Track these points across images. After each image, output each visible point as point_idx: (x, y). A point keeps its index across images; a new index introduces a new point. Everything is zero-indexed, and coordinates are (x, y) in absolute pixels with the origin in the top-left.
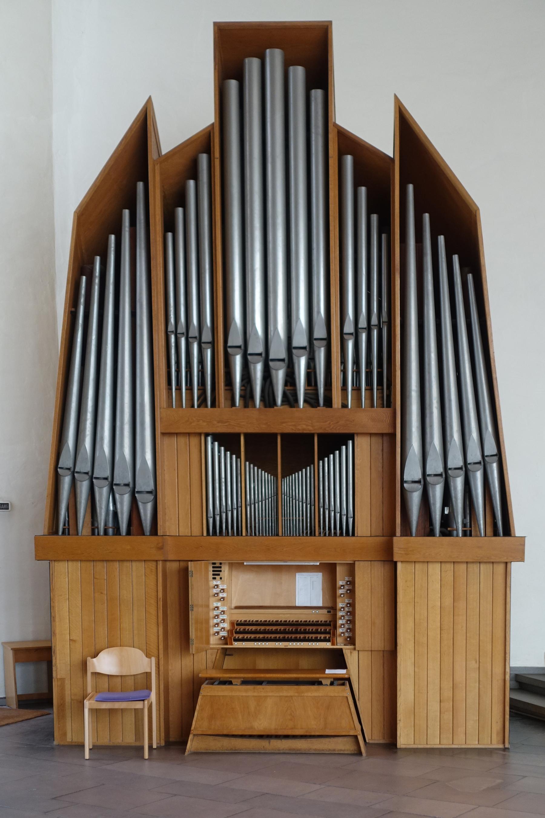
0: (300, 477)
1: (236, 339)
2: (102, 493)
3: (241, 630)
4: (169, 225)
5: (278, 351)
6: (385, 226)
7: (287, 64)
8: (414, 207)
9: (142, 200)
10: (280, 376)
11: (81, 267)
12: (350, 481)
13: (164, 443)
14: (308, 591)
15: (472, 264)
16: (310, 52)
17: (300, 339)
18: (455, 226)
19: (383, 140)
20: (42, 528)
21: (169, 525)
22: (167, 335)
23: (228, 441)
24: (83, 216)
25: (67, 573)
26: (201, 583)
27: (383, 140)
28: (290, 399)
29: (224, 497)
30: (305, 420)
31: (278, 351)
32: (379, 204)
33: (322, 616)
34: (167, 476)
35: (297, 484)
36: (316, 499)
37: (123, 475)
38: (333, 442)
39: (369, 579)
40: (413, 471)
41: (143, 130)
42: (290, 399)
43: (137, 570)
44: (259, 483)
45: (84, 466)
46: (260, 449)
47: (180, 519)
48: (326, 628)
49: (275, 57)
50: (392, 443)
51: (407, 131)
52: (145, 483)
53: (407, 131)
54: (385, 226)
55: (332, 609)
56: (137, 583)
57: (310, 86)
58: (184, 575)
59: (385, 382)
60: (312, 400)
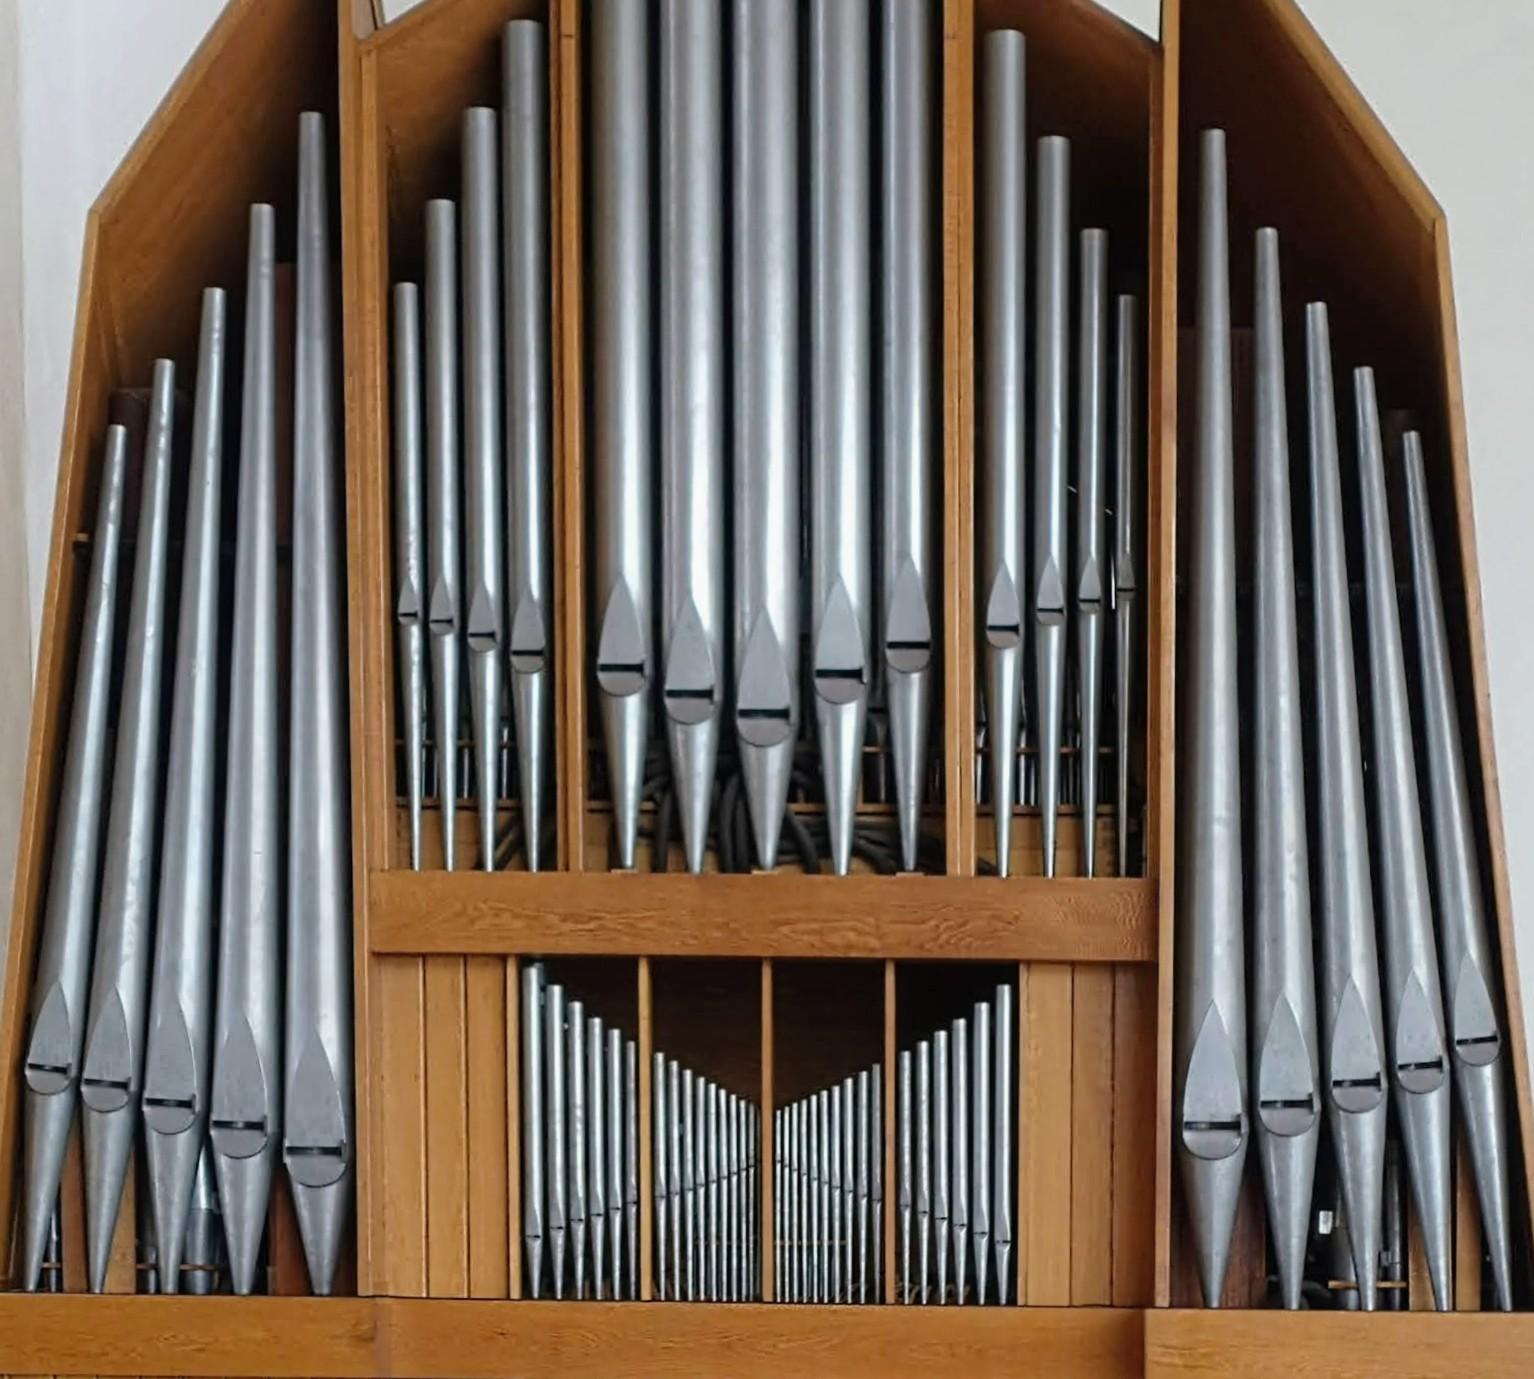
0: (841, 1105)
1: (625, 640)
2: (173, 1152)
4: (407, 259)
5: (767, 682)
6: (1128, 270)
10: (770, 766)
11: (111, 397)
12: (1010, 1121)
13: (392, 993)
15: (1420, 397)
17: (841, 644)
21: (394, 1262)
23: (595, 982)
24: (116, 226)
28: (806, 845)
29: (580, 1176)
30: (852, 914)
32: (1110, 194)
34: (390, 1098)
35: (825, 1132)
36: (890, 1169)
37: (244, 1093)
38: (948, 990)
40: (1213, 1090)
42: (806, 845)
44: (700, 1127)
45: (112, 1060)
46: (702, 1012)
50: (1144, 996)
52: (316, 1120)
54: (1128, 270)
59: (1121, 785)
60: (878, 849)
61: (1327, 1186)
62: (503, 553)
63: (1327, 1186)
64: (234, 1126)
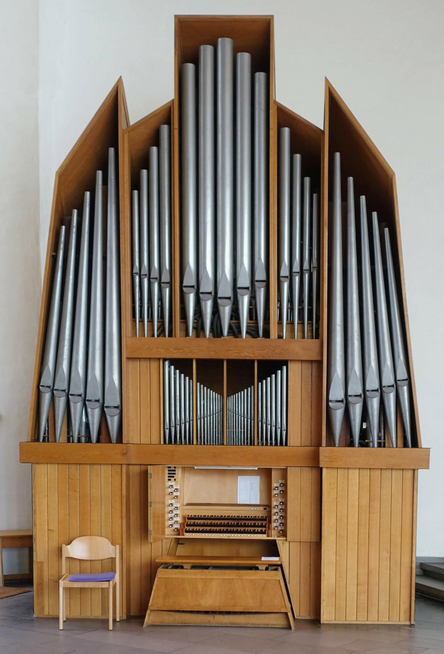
1: (189, 280)
2: (77, 408)
3: (192, 523)
4: (136, 184)
5: (225, 290)
6: (316, 187)
7: (236, 51)
8: (339, 169)
9: (114, 163)
11: (61, 219)
12: (286, 400)
14: (247, 492)
16: (255, 42)
17: (244, 281)
18: (375, 190)
19: (315, 115)
20: (26, 436)
22: (133, 277)
23: (182, 365)
24: (63, 176)
25: (47, 474)
26: (158, 483)
27: (315, 115)
28: (235, 331)
30: (247, 348)
31: (225, 290)
32: (311, 168)
33: (259, 513)
35: (240, 402)
36: (256, 412)
37: (94, 393)
38: (270, 367)
39: (299, 482)
40: (337, 393)
41: (114, 106)
42: (235, 331)
43: (105, 472)
44: (208, 401)
46: (208, 372)
47: (142, 429)
48: (262, 524)
49: (226, 45)
50: (320, 368)
51: (335, 108)
52: (112, 399)
53: (335, 108)
55: (268, 507)
56: (104, 483)
57: (189, 380)
58: (144, 476)
59: (314, 317)
60: (253, 332)
61: (365, 416)
62: (159, 258)
63: (365, 416)
64: (139, 108)
